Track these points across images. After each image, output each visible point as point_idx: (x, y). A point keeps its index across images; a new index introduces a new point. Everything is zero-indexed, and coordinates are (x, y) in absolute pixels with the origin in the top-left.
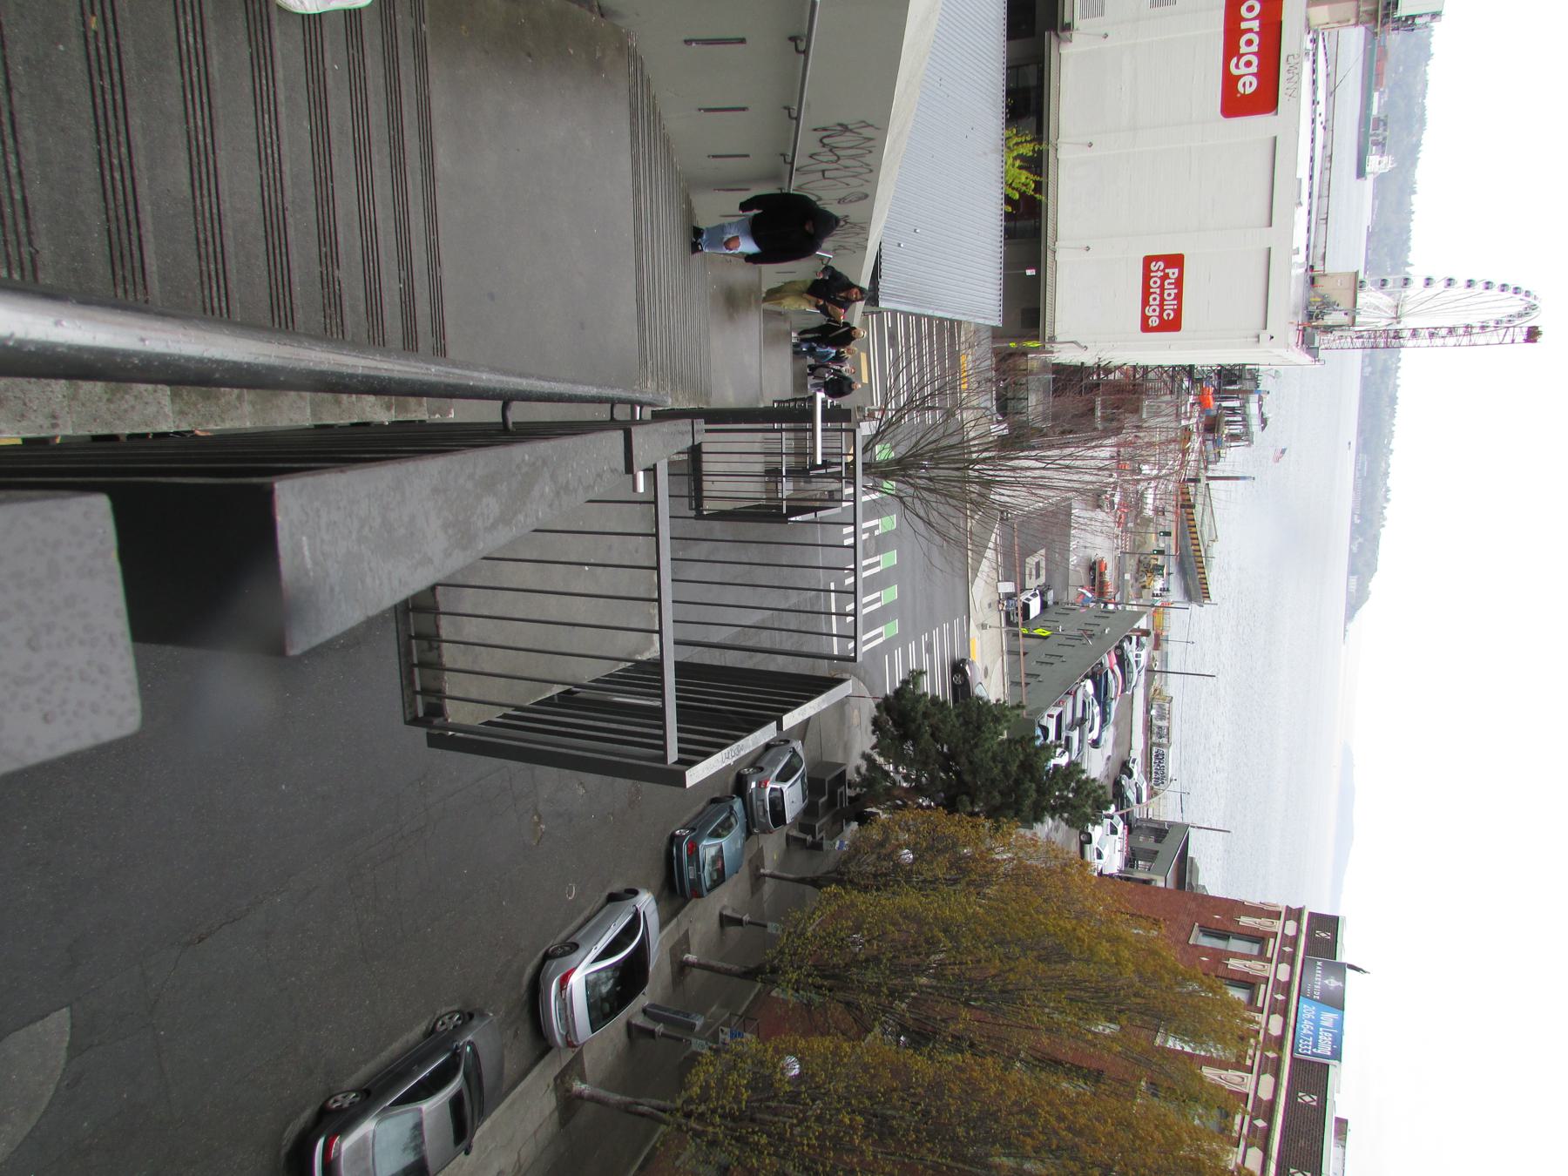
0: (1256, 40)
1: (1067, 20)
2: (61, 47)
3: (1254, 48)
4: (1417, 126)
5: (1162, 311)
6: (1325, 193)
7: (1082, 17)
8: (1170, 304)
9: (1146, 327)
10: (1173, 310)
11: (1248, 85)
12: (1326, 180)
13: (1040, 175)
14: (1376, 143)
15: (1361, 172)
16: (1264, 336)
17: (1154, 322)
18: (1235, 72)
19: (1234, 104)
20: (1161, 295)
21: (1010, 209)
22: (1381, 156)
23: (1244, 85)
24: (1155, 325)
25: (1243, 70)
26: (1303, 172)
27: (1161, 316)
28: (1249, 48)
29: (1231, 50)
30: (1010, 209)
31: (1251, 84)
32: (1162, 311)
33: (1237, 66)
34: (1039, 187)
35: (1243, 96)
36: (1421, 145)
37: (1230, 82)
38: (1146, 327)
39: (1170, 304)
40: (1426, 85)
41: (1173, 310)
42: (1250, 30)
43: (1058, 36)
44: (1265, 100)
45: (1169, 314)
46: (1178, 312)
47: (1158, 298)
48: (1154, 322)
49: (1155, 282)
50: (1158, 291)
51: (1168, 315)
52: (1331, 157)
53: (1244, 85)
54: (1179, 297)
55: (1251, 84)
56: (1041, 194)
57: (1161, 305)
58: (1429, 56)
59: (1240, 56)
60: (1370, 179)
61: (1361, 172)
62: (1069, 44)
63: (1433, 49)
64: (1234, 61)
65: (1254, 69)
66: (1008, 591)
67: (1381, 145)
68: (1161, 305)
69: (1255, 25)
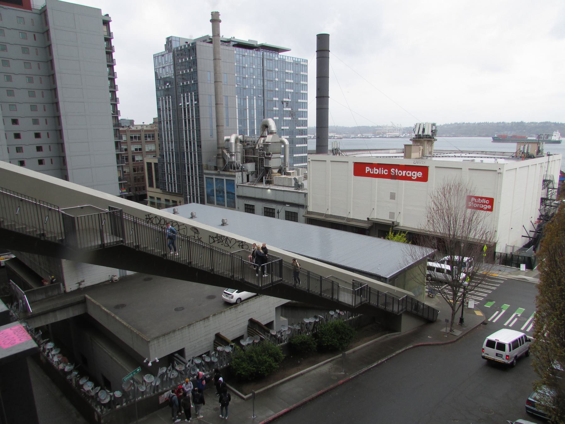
0: (408, 172)
1: (391, 223)
2: (177, 416)
3: (410, 172)
4: (547, 124)
5: (485, 204)
6: (494, 153)
7: (394, 219)
8: (484, 201)
9: (491, 210)
10: (486, 200)
11: (420, 174)
12: (490, 153)
13: (398, 231)
14: (547, 137)
15: (559, 142)
16: (499, 171)
17: (489, 207)
18: (416, 178)
19: (424, 178)
20: (480, 204)
21: (410, 242)
22: (553, 135)
23: (420, 175)
24: (490, 207)
25: (416, 176)
26: (461, 160)
27: (488, 205)
28: (410, 174)
29: (410, 179)
30: (410, 242)
31: (420, 173)
32: (485, 204)
33: (414, 177)
34: (404, 232)
35: (422, 176)
36: (556, 122)
37: (418, 179)
38: (491, 210)
39: (484, 201)
40: (532, 123)
41: (486, 200)
42: (406, 173)
43: (396, 226)
44: (424, 170)
45: (487, 202)
46: (487, 199)
47: (485, 205)
48: (489, 207)
49: (475, 205)
50: (478, 205)
51: (487, 202)
52: (482, 152)
53: (420, 175)
54: (482, 198)
55: (420, 173)
56: (406, 232)
57: (484, 204)
58: (522, 123)
59: (412, 176)
60: (561, 139)
61: (559, 142)
62: (400, 223)
63: (519, 121)
64: (413, 178)
65: (416, 173)
66: (525, 267)
67: (548, 136)
68: (484, 204)
69: (404, 172)
